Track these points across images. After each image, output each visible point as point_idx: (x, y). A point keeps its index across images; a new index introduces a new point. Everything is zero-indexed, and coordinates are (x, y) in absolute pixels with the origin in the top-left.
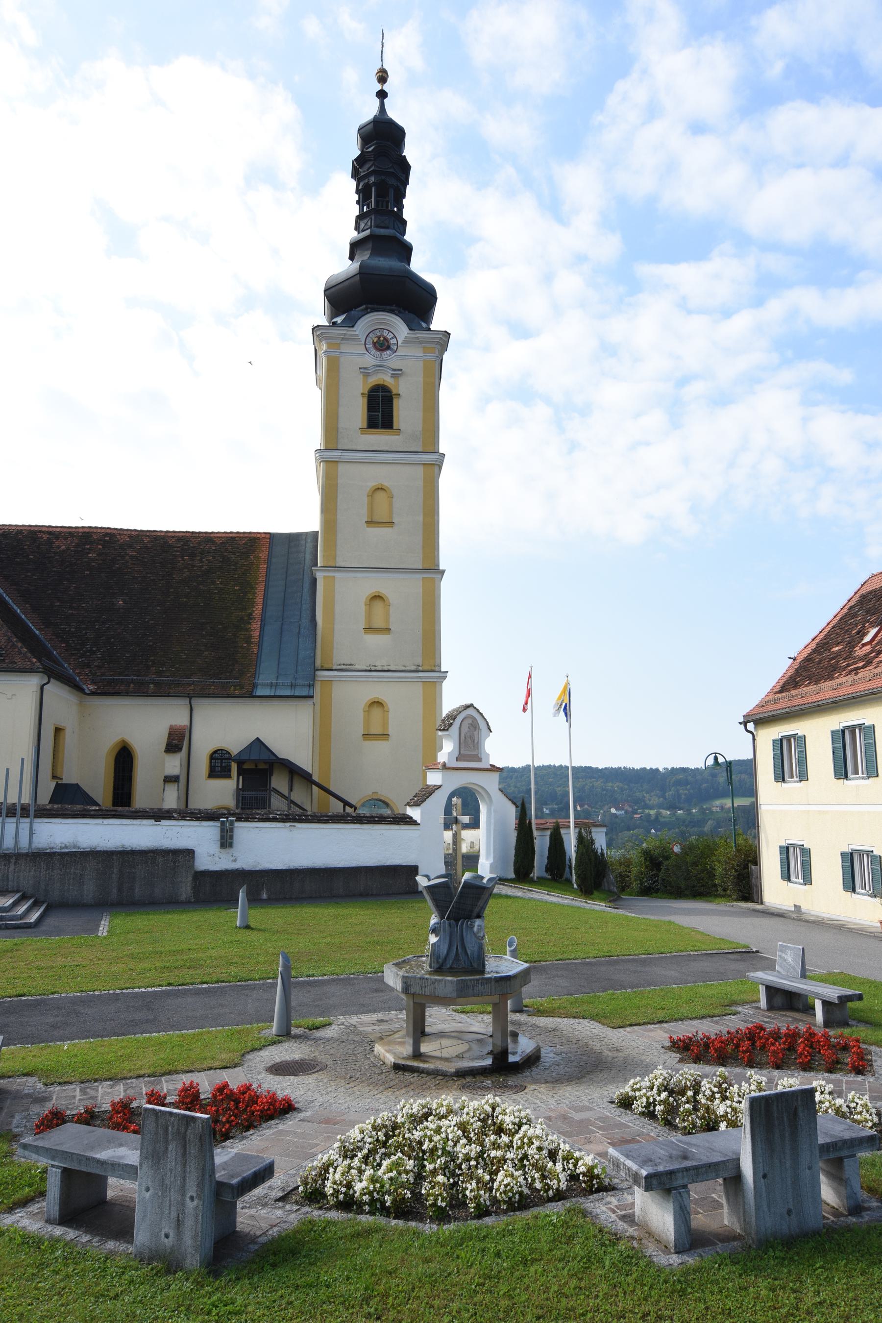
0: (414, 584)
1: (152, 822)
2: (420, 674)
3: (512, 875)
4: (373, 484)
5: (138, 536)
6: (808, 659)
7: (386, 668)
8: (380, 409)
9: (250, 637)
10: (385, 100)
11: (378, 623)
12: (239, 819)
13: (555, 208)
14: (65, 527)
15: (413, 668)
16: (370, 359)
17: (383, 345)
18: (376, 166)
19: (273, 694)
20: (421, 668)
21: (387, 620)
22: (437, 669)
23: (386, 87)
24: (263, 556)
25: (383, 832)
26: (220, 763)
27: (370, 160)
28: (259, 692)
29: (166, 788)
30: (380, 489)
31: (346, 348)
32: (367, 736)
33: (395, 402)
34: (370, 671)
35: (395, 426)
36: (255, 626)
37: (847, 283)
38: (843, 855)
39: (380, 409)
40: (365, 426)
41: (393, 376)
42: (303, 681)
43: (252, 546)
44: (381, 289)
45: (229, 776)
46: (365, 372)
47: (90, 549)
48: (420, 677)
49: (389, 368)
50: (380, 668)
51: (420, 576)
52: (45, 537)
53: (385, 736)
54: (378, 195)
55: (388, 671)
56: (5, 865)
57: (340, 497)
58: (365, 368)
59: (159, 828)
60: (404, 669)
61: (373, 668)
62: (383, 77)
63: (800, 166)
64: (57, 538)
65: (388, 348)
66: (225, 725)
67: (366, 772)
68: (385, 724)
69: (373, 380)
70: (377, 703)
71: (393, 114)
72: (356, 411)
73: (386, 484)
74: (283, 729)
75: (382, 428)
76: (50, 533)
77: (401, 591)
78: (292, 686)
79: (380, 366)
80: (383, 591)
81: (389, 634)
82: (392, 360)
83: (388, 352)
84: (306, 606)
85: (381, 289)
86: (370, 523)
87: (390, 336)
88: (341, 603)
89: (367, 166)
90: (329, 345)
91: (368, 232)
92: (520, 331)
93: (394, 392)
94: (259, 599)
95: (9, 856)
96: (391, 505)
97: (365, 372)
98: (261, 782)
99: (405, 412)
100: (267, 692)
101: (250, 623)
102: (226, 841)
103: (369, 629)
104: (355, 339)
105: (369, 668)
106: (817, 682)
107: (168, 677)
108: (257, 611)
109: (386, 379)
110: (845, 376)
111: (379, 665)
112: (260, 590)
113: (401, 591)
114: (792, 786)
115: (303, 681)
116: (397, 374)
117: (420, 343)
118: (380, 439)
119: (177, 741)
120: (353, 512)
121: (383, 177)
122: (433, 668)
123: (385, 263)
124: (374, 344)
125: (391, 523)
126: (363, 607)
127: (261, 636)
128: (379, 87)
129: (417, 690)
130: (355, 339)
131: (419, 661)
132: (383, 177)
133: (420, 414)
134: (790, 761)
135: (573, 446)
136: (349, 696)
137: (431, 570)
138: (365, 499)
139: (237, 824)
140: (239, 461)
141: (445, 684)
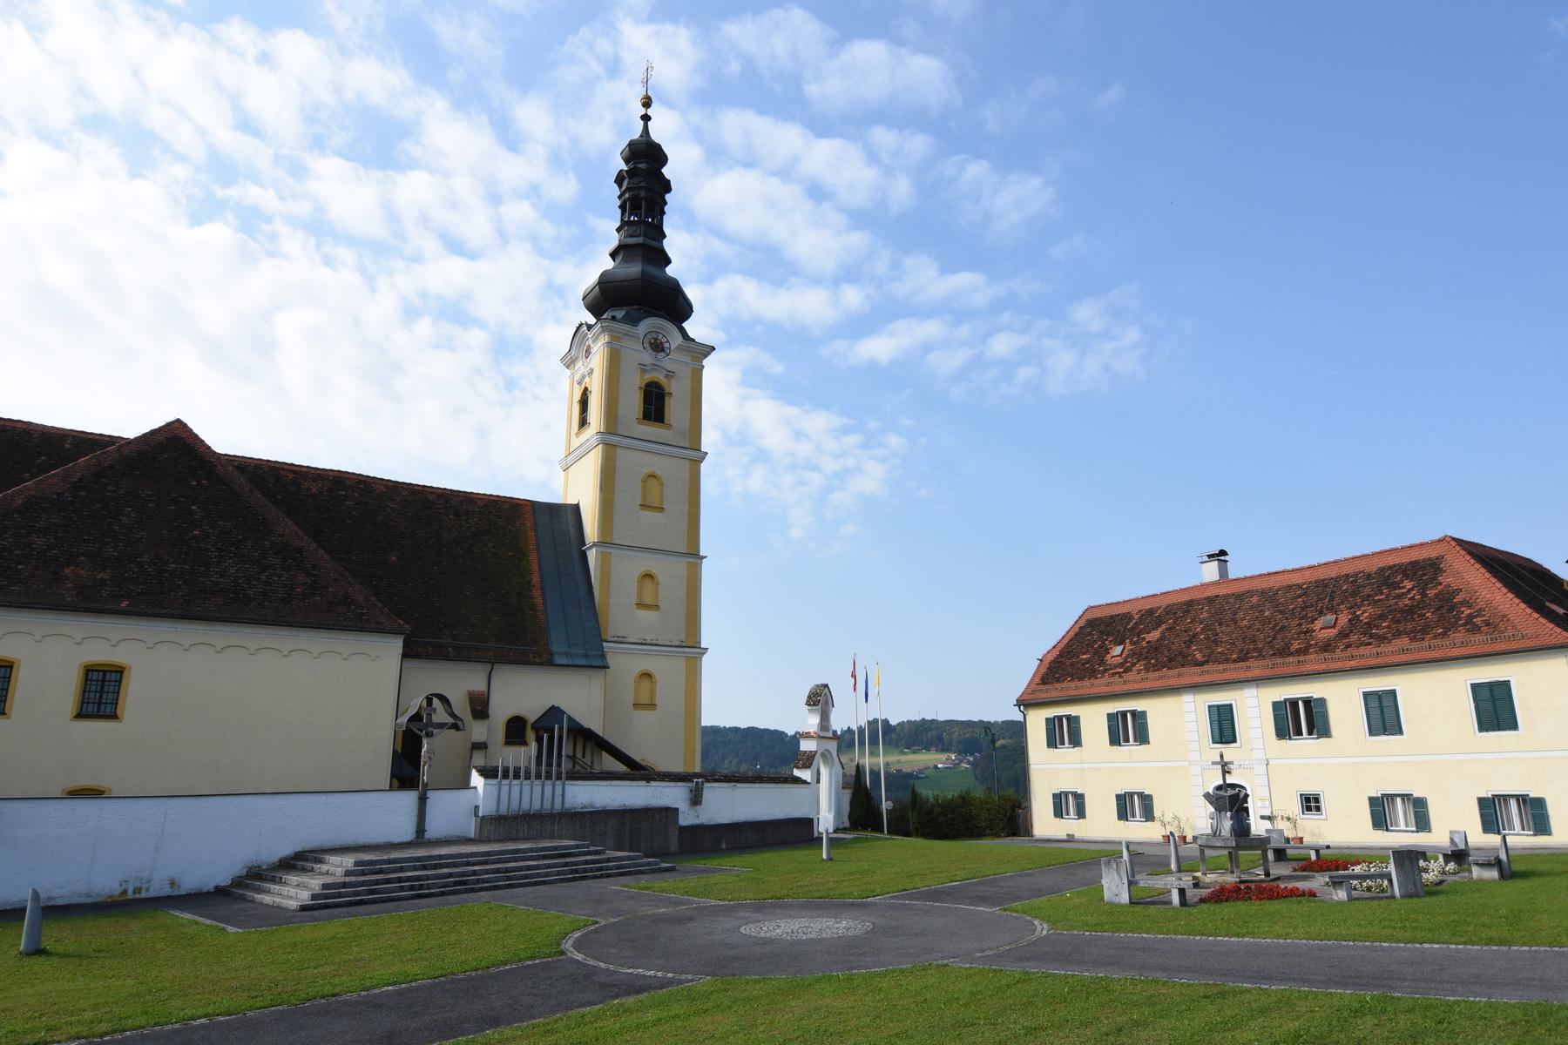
3: (847, 824)
4: (647, 471)
6: (1055, 661)
8: (654, 403)
12: (708, 781)
13: (509, 137)
16: (647, 357)
17: (658, 347)
21: (656, 598)
23: (650, 112)
24: (529, 523)
26: (516, 730)
28: (558, 660)
30: (653, 476)
31: (626, 343)
32: (637, 706)
33: (667, 399)
36: (536, 593)
37: (778, 283)
38: (1118, 797)
39: (654, 403)
42: (591, 654)
44: (640, 295)
45: (524, 743)
46: (644, 368)
51: (684, 560)
52: (291, 476)
53: (652, 706)
62: (647, 103)
63: (749, 165)
66: (522, 692)
67: (643, 737)
68: (652, 693)
69: (649, 377)
70: (647, 675)
71: (656, 135)
72: (633, 403)
73: (658, 472)
74: (577, 696)
76: (295, 472)
77: (668, 571)
78: (586, 656)
80: (654, 571)
82: (667, 363)
85: (640, 295)
86: (644, 506)
88: (615, 581)
89: (636, 180)
90: (612, 338)
91: (640, 240)
92: (456, 246)
94: (535, 567)
97: (644, 368)
98: (571, 745)
99: (675, 409)
100: (564, 661)
102: (696, 799)
103: (640, 605)
104: (637, 338)
106: (1081, 679)
108: (536, 578)
109: (660, 377)
110: (779, 368)
111: (650, 638)
112: (533, 557)
113: (668, 571)
114: (1066, 752)
115: (591, 654)
116: (670, 375)
118: (652, 430)
119: (480, 707)
120: (629, 495)
125: (661, 509)
127: (545, 604)
128: (643, 111)
129: (679, 664)
134: (1064, 733)
135: (511, 385)
136: (625, 663)
137: (693, 555)
138: (640, 485)
141: (705, 658)
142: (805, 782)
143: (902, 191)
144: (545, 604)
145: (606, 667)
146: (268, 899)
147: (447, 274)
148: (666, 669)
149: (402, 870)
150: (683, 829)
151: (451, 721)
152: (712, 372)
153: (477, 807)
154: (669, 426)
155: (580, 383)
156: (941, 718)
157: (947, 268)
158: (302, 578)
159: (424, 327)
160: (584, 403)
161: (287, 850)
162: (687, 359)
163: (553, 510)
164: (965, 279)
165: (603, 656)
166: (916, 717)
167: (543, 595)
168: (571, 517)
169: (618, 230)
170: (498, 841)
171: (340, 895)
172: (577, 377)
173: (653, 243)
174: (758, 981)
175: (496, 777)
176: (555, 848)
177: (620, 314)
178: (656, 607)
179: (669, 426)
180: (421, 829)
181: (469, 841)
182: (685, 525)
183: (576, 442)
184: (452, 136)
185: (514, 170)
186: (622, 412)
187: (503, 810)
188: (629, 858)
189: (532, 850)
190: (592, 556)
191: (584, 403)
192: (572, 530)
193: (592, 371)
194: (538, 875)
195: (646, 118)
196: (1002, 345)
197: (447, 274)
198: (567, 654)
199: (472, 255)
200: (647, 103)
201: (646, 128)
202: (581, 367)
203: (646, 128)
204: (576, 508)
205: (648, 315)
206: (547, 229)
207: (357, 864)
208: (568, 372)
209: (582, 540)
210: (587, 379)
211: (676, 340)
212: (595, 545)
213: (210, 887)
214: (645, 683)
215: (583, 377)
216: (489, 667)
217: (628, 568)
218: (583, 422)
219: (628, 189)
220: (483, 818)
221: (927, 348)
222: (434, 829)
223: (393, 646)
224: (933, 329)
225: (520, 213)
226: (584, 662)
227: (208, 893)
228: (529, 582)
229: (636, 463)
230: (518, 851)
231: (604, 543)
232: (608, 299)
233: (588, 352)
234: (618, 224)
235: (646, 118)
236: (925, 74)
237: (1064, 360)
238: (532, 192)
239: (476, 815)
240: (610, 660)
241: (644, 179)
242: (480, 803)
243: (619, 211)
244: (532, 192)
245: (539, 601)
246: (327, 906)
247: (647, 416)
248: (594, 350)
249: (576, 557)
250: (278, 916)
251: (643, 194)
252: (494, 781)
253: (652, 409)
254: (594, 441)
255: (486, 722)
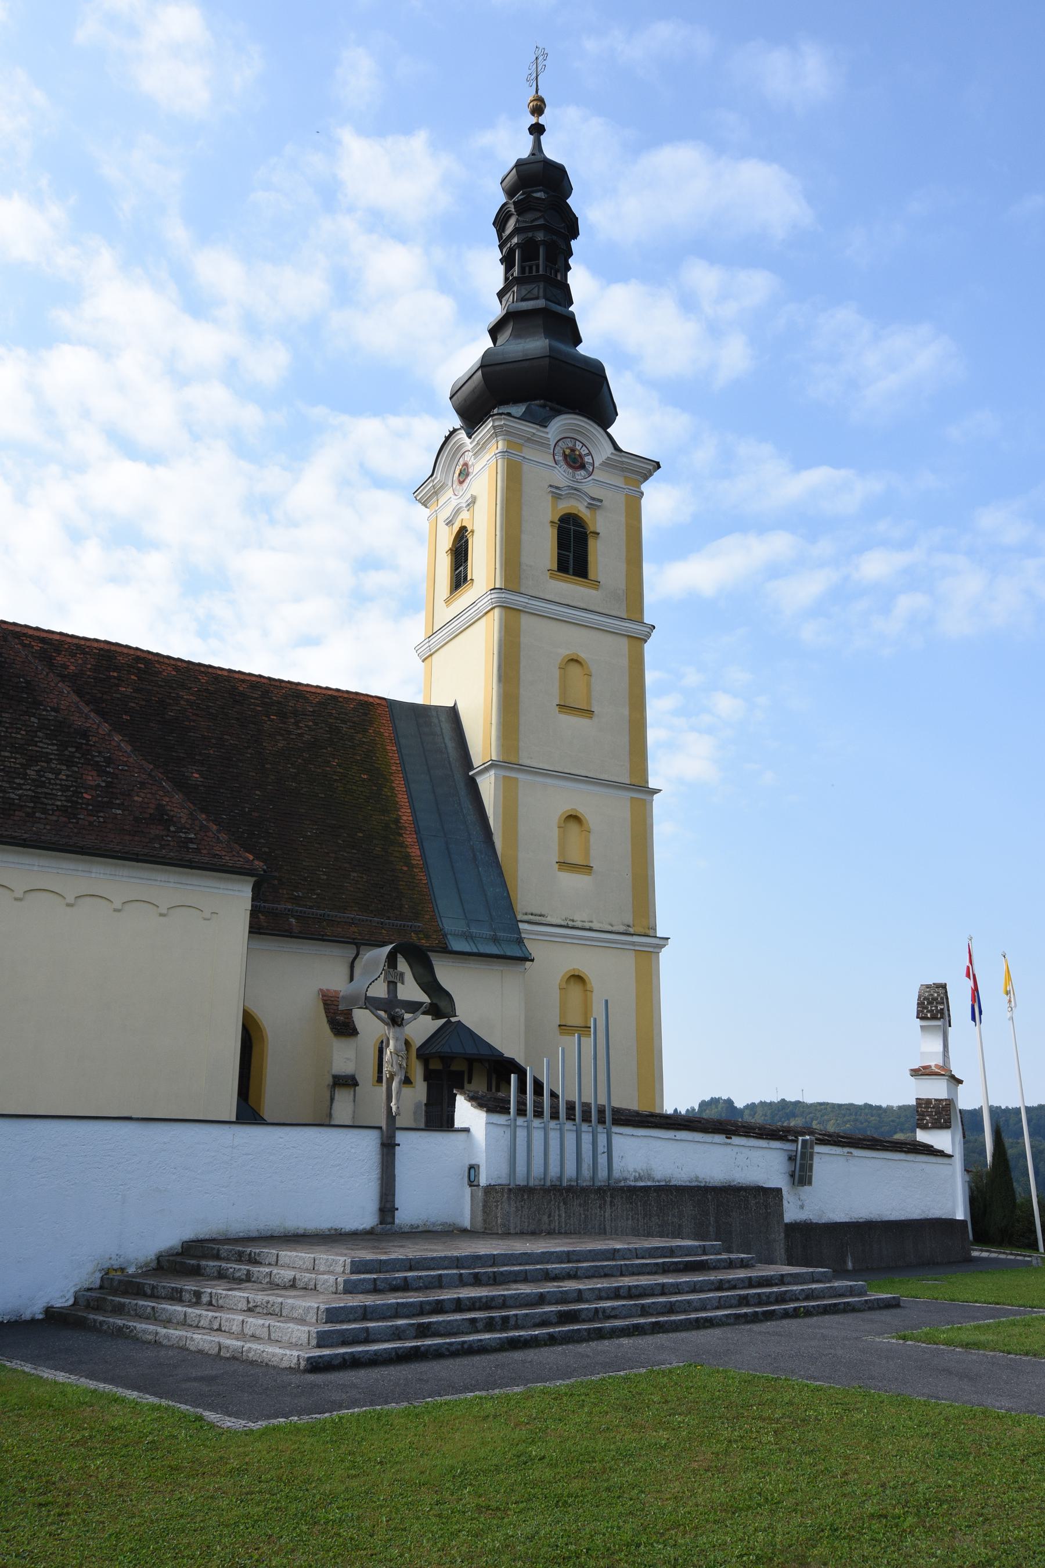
0: (619, 805)
1: (720, 1138)
2: (636, 939)
4: (565, 652)
5: (188, 669)
7: (587, 925)
9: (407, 856)
10: (542, 137)
11: (576, 858)
13: (197, 304)
14: (67, 635)
15: (622, 929)
16: (561, 475)
17: (575, 462)
18: (545, 220)
19: (475, 950)
20: (631, 930)
22: (651, 933)
23: (542, 120)
25: (924, 1166)
27: (540, 211)
29: (337, 1096)
30: (575, 661)
31: (529, 453)
33: (591, 542)
34: (567, 927)
35: (591, 575)
36: (409, 839)
40: (556, 568)
41: (590, 506)
43: (366, 714)
44: (539, 381)
46: (556, 493)
47: (118, 678)
48: (633, 943)
49: (586, 494)
50: (579, 924)
52: (37, 646)
54: (523, 259)
55: (590, 930)
56: (600, 1207)
57: (523, 663)
58: (557, 488)
59: (729, 1149)
60: (610, 928)
61: (571, 924)
64: (58, 652)
65: (583, 466)
69: (566, 506)
71: (551, 153)
72: (542, 547)
73: (583, 655)
75: (574, 575)
76: (43, 640)
78: (495, 940)
79: (576, 489)
80: (582, 810)
81: (589, 874)
83: (583, 472)
84: (472, 817)
85: (539, 381)
86: (563, 707)
87: (584, 451)
88: (525, 822)
89: (529, 216)
90: (509, 443)
91: (540, 303)
92: (127, 447)
93: (591, 528)
94: (402, 798)
95: (605, 1191)
96: (589, 685)
97: (556, 493)
99: (603, 555)
101: (401, 835)
103: (565, 865)
105: (563, 923)
107: (311, 907)
109: (580, 508)
112: (398, 783)
116: (595, 504)
117: (623, 470)
118: (568, 589)
120: (541, 690)
121: (530, 235)
122: (647, 931)
123: (535, 345)
124: (565, 456)
125: (588, 713)
126: (556, 831)
127: (423, 855)
128: (533, 120)
129: (627, 962)
130: (542, 444)
131: (629, 919)
132: (555, 238)
133: (623, 567)
136: (552, 959)
137: (640, 790)
138: (557, 673)
139: (818, 1149)
140: (330, 578)
141: (664, 955)
142: (941, 1154)
143: (735, 356)
144: (423, 855)
145: (527, 958)
146: (200, 1340)
147: (120, 483)
148: (607, 970)
149: (439, 1283)
150: (786, 1225)
151: (424, 998)
152: (658, 502)
153: (473, 1168)
154: (596, 584)
155: (450, 523)
156: (810, 1099)
157: (800, 465)
158: (91, 778)
159: (92, 553)
160: (460, 552)
161: (168, 1236)
162: (618, 481)
163: (419, 713)
164: (817, 476)
165: (520, 941)
166: (773, 1097)
167: (420, 842)
168: (446, 727)
169: (501, 295)
170: (522, 1234)
171: (367, 1337)
172: (445, 513)
173: (559, 309)
174: (356, 1476)
175: (506, 1111)
176: (671, 1252)
177: (519, 410)
178: (587, 869)
179: (596, 584)
180: (387, 1208)
181: (452, 1232)
182: (626, 739)
183: (445, 613)
184: (125, 303)
185: (205, 343)
186: (526, 559)
187: (521, 1181)
188: (797, 1279)
189: (637, 1254)
190: (488, 786)
191: (460, 552)
192: (451, 745)
193: (473, 500)
194: (689, 1307)
195: (537, 130)
196: (875, 566)
197: (120, 483)
198: (469, 937)
199: (153, 458)
200: (538, 109)
201: (538, 145)
202: (450, 500)
203: (538, 145)
204: (453, 712)
205: (559, 413)
206: (251, 416)
207: (358, 1267)
208: (426, 512)
209: (466, 760)
210: (465, 515)
211: (602, 453)
212: (493, 765)
213: (35, 1310)
214: (575, 990)
215: (457, 511)
216: (351, 951)
217: (544, 806)
218: (459, 579)
219: (516, 231)
220: (489, 1189)
221: (775, 571)
222: (411, 1209)
223: (232, 902)
224: (780, 544)
225: (215, 399)
226: (494, 950)
227: (33, 1321)
228: (397, 821)
229: (550, 641)
230: (613, 1254)
231: (507, 764)
232: (484, 399)
233: (464, 474)
234: (500, 285)
235: (537, 130)
236: (766, 193)
237: (968, 584)
238: (231, 373)
239: (472, 1183)
240: (532, 948)
241: (539, 217)
242: (481, 1159)
243: (501, 269)
244: (231, 373)
245: (415, 851)
246: (354, 1363)
247: (563, 567)
248: (474, 470)
249: (462, 791)
250: (233, 1380)
251: (540, 236)
252: (501, 1119)
253: (575, 549)
254: (485, 603)
255: (397, 1029)
